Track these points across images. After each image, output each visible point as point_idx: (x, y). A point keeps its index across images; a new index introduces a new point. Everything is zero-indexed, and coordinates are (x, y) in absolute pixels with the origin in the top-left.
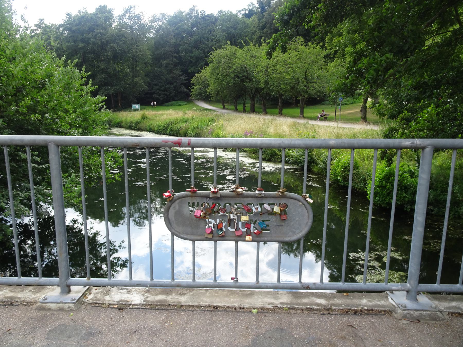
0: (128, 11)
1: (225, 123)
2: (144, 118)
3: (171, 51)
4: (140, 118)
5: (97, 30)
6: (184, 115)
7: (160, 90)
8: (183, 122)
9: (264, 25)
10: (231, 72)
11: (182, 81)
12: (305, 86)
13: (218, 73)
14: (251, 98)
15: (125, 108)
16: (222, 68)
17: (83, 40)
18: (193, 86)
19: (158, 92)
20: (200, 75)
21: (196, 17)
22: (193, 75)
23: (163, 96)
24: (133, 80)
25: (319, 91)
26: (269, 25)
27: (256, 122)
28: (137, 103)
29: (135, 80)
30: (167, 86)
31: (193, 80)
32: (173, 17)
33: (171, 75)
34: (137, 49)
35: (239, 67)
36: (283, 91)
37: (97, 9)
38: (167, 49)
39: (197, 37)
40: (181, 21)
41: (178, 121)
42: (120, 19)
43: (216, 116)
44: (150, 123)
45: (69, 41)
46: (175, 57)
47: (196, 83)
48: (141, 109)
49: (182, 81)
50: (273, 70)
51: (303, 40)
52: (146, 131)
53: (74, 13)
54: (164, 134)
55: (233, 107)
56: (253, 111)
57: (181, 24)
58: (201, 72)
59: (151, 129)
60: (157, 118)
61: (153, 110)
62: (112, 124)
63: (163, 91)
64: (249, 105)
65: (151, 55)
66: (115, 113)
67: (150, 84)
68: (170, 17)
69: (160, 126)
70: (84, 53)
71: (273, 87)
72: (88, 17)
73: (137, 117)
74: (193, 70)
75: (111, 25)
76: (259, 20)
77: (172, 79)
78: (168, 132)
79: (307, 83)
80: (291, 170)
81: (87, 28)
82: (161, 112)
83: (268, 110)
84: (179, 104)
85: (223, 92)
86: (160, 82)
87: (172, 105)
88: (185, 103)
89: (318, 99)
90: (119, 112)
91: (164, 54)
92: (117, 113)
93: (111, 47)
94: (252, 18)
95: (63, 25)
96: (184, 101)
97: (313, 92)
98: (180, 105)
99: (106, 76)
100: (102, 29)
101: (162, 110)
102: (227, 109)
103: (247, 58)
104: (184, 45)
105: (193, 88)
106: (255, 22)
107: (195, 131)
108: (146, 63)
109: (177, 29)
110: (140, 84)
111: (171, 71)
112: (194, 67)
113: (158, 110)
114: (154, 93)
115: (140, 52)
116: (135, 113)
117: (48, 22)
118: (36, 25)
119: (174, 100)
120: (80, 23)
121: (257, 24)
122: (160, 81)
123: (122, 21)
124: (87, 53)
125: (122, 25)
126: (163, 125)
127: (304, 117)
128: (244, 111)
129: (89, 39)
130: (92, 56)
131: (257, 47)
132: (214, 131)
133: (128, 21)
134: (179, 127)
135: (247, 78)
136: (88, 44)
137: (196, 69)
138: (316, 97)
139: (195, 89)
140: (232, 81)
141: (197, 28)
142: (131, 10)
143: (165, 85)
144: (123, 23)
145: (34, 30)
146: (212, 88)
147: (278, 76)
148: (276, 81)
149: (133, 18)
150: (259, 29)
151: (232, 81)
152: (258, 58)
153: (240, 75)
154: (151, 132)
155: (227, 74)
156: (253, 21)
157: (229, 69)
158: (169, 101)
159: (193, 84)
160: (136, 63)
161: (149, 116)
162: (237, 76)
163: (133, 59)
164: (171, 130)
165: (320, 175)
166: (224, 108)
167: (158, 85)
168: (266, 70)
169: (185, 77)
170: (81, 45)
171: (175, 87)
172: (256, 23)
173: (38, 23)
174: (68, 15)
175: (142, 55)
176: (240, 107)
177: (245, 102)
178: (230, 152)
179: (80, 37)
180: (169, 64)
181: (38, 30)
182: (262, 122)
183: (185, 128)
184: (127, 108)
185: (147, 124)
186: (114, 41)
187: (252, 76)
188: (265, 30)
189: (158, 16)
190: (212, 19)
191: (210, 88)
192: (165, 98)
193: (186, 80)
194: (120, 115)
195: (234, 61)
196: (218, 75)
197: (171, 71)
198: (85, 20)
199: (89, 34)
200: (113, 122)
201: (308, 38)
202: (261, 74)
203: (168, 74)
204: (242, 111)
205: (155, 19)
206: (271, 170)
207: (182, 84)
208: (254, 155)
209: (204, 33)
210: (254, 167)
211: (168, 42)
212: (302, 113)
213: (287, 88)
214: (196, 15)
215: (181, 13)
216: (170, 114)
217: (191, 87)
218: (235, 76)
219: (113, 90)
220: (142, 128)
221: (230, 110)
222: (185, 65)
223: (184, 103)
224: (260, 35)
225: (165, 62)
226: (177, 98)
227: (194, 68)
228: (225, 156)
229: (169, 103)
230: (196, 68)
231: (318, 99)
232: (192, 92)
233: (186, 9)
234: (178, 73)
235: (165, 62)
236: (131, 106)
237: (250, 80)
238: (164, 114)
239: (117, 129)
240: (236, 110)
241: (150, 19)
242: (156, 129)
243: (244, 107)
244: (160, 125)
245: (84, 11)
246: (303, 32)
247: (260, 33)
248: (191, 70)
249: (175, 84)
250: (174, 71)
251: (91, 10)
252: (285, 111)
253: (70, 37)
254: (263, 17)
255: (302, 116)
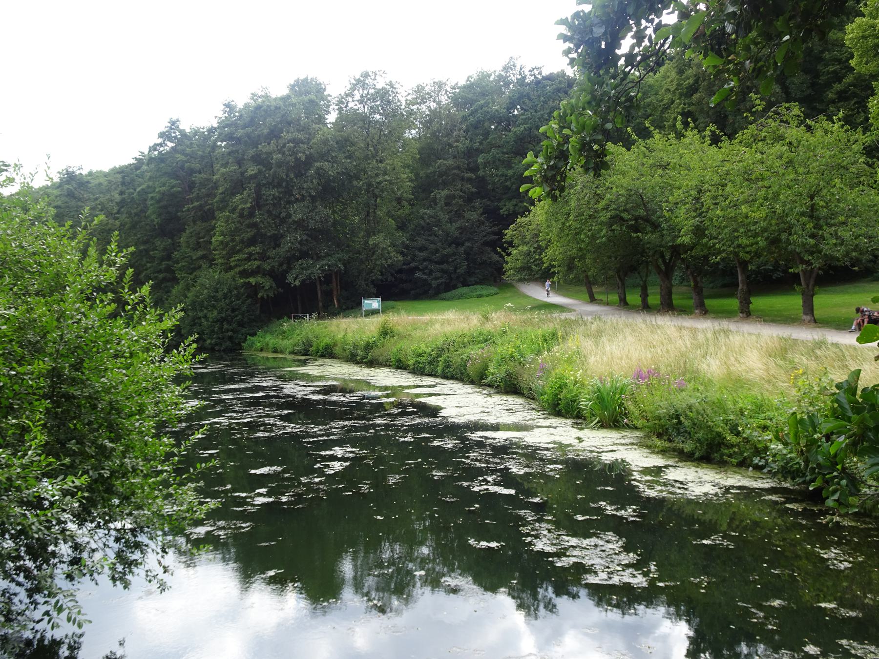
0: (360, 83)
1: (588, 345)
2: (385, 332)
3: (458, 168)
4: (376, 334)
5: (288, 132)
6: (482, 324)
7: (431, 261)
8: (479, 342)
9: (694, 84)
10: (604, 209)
11: (485, 236)
12: (813, 236)
13: (568, 214)
14: (659, 271)
15: (348, 309)
16: (578, 199)
17: (257, 159)
18: (510, 249)
19: (426, 267)
20: (528, 219)
21: (522, 81)
22: (510, 219)
23: (439, 274)
24: (366, 243)
25: (856, 248)
26: (706, 83)
27: (670, 340)
28: (376, 296)
29: (371, 243)
30: (448, 250)
31: (509, 233)
32: (465, 87)
33: (458, 224)
34: (378, 168)
35: (622, 195)
36: (747, 252)
37: (292, 87)
38: (450, 162)
39: (522, 128)
40: (483, 94)
41: (466, 340)
42: (340, 102)
43: (566, 323)
44: (399, 346)
45: (227, 163)
46: (470, 180)
47: (516, 242)
48: (384, 311)
49: (485, 236)
50: (715, 198)
51: (799, 113)
52: (389, 366)
53: (241, 101)
54: (430, 375)
55: (615, 298)
56: (668, 306)
57: (482, 102)
58: (529, 211)
59: (399, 361)
60: (418, 333)
61: (408, 312)
62: (311, 349)
63: (437, 263)
64: (657, 289)
65: (411, 181)
66: (321, 322)
67: (407, 247)
68: (458, 88)
69: (420, 355)
70: (259, 186)
71: (716, 241)
72: (268, 106)
73: (371, 331)
74: (512, 208)
75: (321, 120)
76: (681, 72)
77: (461, 233)
78: (440, 369)
79: (818, 227)
80: (774, 498)
81: (266, 131)
82: (427, 317)
83: (708, 302)
84: (478, 293)
85: (582, 258)
86: (432, 242)
87: (460, 297)
88: (494, 289)
89: (856, 268)
90: (332, 318)
91: (441, 175)
92: (327, 322)
93: (318, 169)
94: (662, 69)
95: (215, 129)
96: (490, 285)
97: (839, 252)
98: (481, 296)
99: (305, 238)
100: (298, 131)
101: (432, 311)
102: (600, 302)
103: (643, 170)
104: (489, 152)
105: (509, 254)
106: (669, 80)
107: (504, 368)
108: (399, 200)
109: (472, 114)
110: (384, 249)
111: (459, 215)
112: (514, 202)
113: (422, 312)
114: (417, 269)
115: (385, 173)
116: (367, 320)
117: (186, 126)
118: (162, 135)
119: (465, 284)
120: (252, 122)
121: (675, 83)
122: (431, 238)
123: (346, 107)
124: (264, 185)
125: (348, 119)
126: (428, 350)
127: (815, 321)
128: (646, 307)
129: (269, 154)
130: (275, 192)
131: (674, 141)
132: (554, 368)
133: (359, 106)
134: (465, 357)
135: (647, 220)
136: (269, 166)
137: (520, 204)
138: (848, 263)
139: (516, 256)
140: (604, 231)
141: (522, 108)
142: (367, 82)
143: (444, 249)
144: (346, 111)
145: (158, 145)
146: (554, 253)
147: (731, 213)
148: (726, 227)
149: (369, 99)
150: (681, 95)
151: (604, 231)
152: (674, 168)
153: (625, 216)
154: (401, 368)
155: (590, 216)
156: (665, 77)
157: (598, 202)
158: (455, 287)
159: (511, 244)
160: (376, 201)
161: (400, 329)
162: (617, 219)
163: (368, 192)
164: (448, 365)
165: (870, 516)
166: (593, 300)
167: (427, 249)
168: (697, 199)
169: (494, 226)
170: (252, 170)
171: (467, 253)
172: (672, 81)
173: (167, 129)
174: (227, 105)
175: (390, 182)
176: (634, 298)
177: (645, 282)
178: (593, 428)
179: (251, 152)
180: (454, 197)
181: (166, 145)
182: (688, 343)
183: (482, 357)
184: (352, 308)
185: (392, 348)
186: (323, 157)
187: (660, 217)
188: (696, 96)
189: (427, 89)
190: (560, 82)
191: (550, 252)
192: (443, 280)
193: (494, 233)
194: (333, 328)
195: (609, 180)
196: (567, 219)
197: (459, 215)
198: (263, 113)
199: (269, 144)
200: (315, 344)
201: (818, 105)
202: (682, 211)
203: (451, 221)
204: (638, 307)
205: (421, 95)
206: (706, 494)
207: (486, 244)
208: (659, 443)
209: (539, 118)
210: (658, 483)
211: (451, 146)
212: (809, 308)
213: (757, 243)
214: (519, 77)
215: (484, 76)
216: (449, 322)
217: (504, 249)
218: (612, 217)
219: (319, 268)
220: (381, 359)
221: (608, 304)
222: (495, 197)
223: (492, 291)
224: (683, 109)
225: (445, 192)
226: (472, 279)
227: (515, 203)
228: (575, 442)
229: (454, 292)
230: (521, 202)
231: (856, 268)
232: (507, 263)
233: (494, 66)
234: (476, 217)
235: (445, 192)
236: (360, 304)
237: (656, 226)
238: (432, 323)
239: (320, 362)
240: (624, 304)
241: (409, 98)
242: (411, 362)
243: (644, 295)
244: (420, 351)
245: (263, 93)
246: (803, 91)
247: (685, 104)
248: (507, 207)
249: (467, 244)
250: (465, 215)
251: (279, 90)
252: (759, 302)
253: (229, 154)
254: (690, 66)
255: (808, 318)
